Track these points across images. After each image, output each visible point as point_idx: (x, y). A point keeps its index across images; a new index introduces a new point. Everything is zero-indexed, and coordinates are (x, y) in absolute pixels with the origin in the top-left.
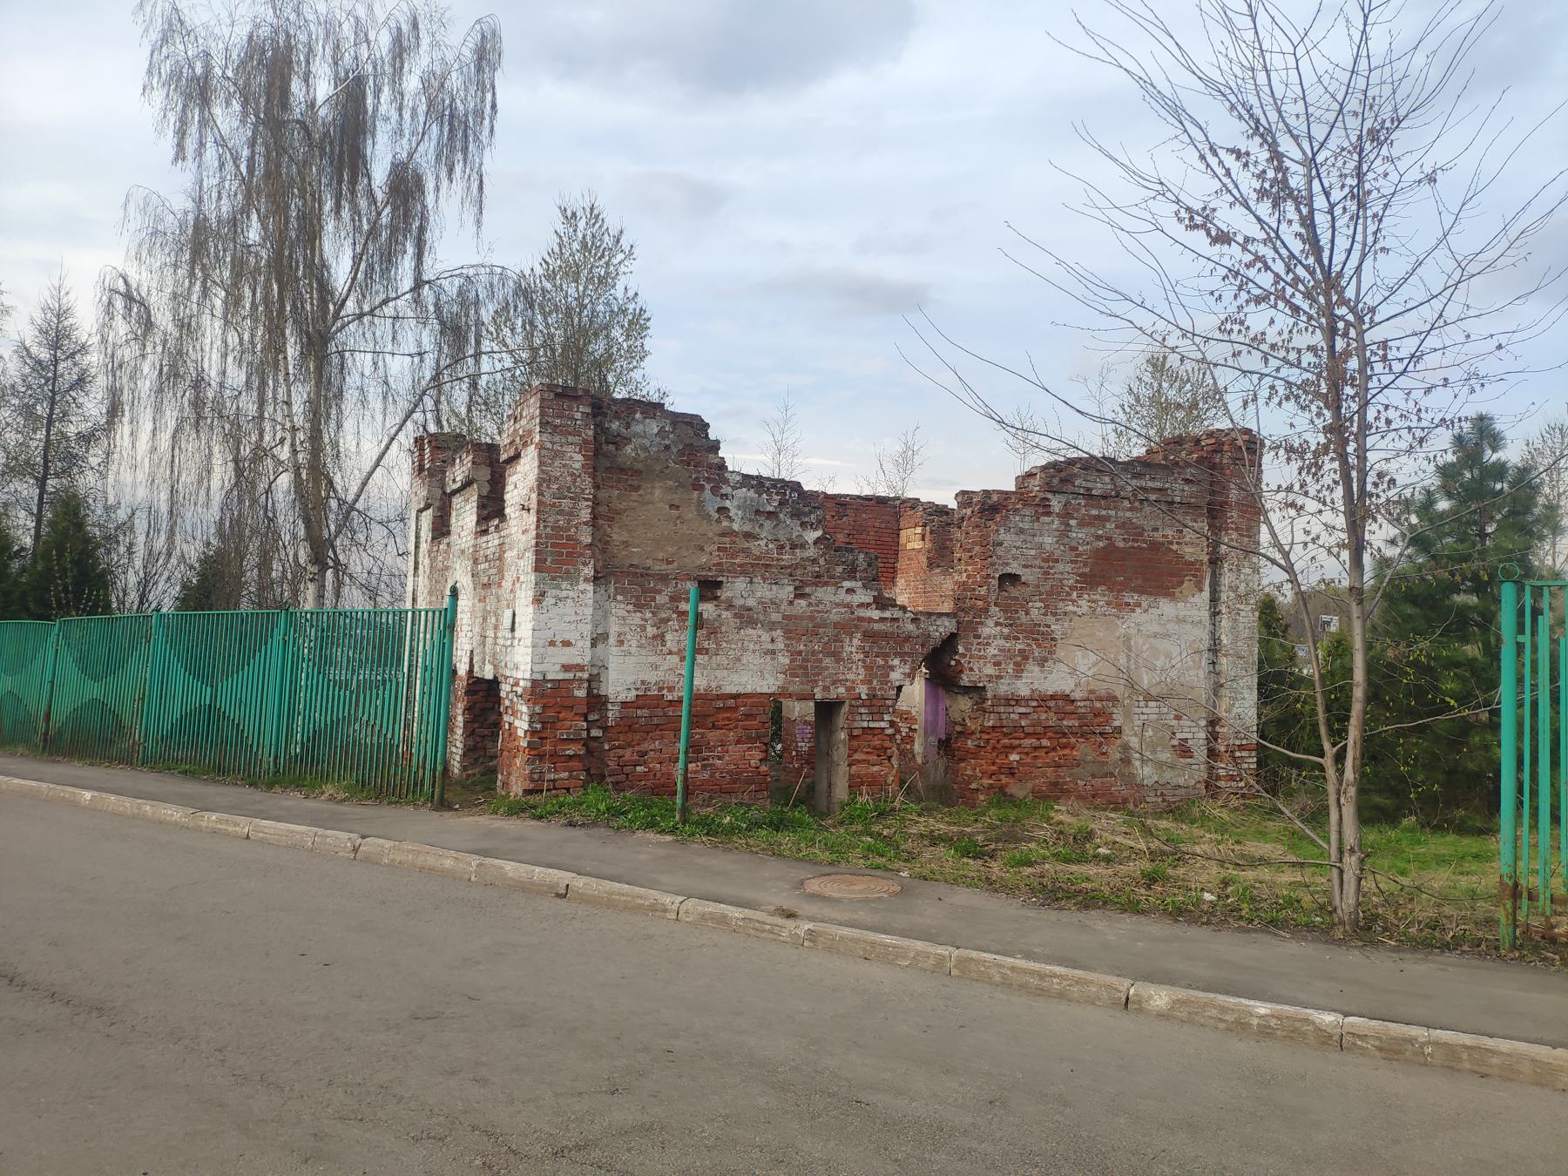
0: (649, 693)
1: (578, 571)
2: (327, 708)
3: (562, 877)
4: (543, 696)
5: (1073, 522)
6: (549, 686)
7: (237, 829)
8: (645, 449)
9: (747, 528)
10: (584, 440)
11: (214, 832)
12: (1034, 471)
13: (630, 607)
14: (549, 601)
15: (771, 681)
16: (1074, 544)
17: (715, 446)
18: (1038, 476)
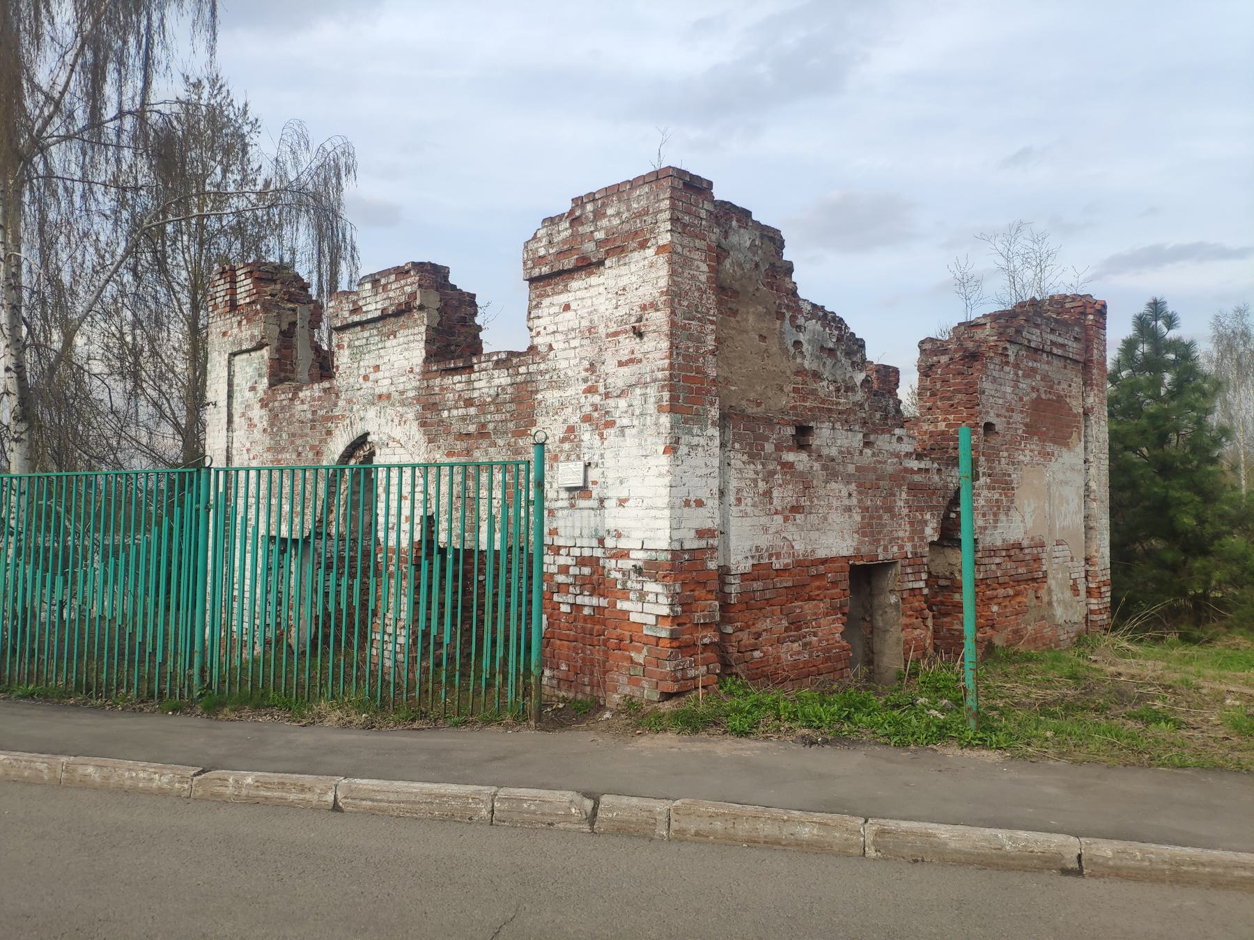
0: (762, 561)
1: (706, 412)
2: (442, 605)
3: (1067, 846)
4: (681, 571)
5: (1020, 373)
6: (687, 557)
7: (308, 796)
8: (740, 265)
9: (814, 366)
10: (709, 246)
11: (253, 802)
12: (983, 321)
13: (745, 458)
14: (683, 450)
15: (849, 542)
16: (1021, 394)
17: (789, 269)
18: (988, 326)
